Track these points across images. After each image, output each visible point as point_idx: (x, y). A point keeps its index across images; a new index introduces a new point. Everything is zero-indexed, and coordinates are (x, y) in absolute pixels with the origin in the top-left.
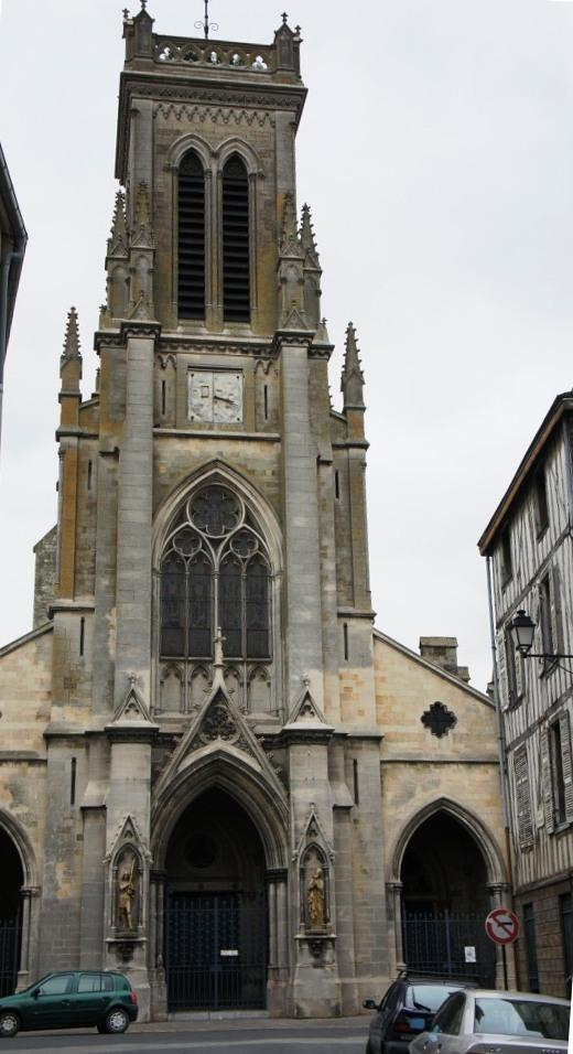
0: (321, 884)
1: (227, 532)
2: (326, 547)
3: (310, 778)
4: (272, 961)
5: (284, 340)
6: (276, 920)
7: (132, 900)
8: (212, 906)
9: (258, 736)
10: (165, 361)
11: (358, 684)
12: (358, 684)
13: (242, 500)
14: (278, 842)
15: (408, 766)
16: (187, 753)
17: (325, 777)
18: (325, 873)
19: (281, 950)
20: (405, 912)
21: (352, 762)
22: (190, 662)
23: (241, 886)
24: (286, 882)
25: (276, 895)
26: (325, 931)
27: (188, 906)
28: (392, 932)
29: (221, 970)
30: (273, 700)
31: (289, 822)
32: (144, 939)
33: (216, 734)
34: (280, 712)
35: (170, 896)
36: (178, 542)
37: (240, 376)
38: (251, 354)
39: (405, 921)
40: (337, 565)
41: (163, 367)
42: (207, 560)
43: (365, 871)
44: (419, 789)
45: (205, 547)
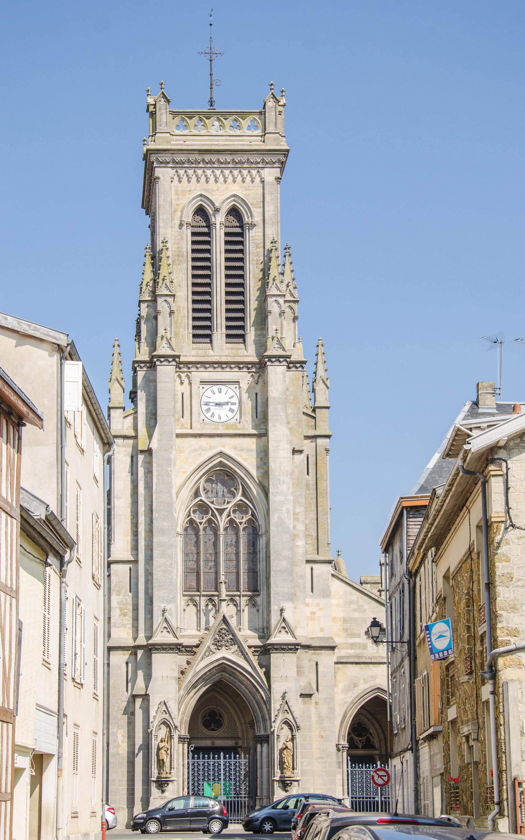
0: (290, 745)
1: (228, 503)
2: (298, 514)
3: (284, 675)
4: (259, 794)
5: (269, 361)
6: (262, 768)
7: (167, 754)
8: (219, 758)
9: (250, 647)
10: (183, 378)
11: (320, 609)
12: (320, 609)
13: (239, 480)
14: (263, 717)
15: (354, 665)
16: (202, 658)
17: (295, 674)
18: (293, 739)
19: (265, 787)
20: (349, 763)
21: (315, 663)
22: (203, 596)
23: (240, 743)
24: (268, 743)
25: (262, 752)
26: (292, 775)
27: (204, 758)
28: (339, 777)
29: (225, 798)
30: (261, 620)
31: (270, 705)
32: (175, 779)
33: (221, 646)
34: (265, 630)
35: (192, 751)
36: (195, 511)
37: (237, 386)
38: (245, 370)
39: (349, 769)
40: (306, 525)
41: (182, 383)
42: (215, 524)
43: (322, 737)
44: (361, 681)
45: (213, 515)
